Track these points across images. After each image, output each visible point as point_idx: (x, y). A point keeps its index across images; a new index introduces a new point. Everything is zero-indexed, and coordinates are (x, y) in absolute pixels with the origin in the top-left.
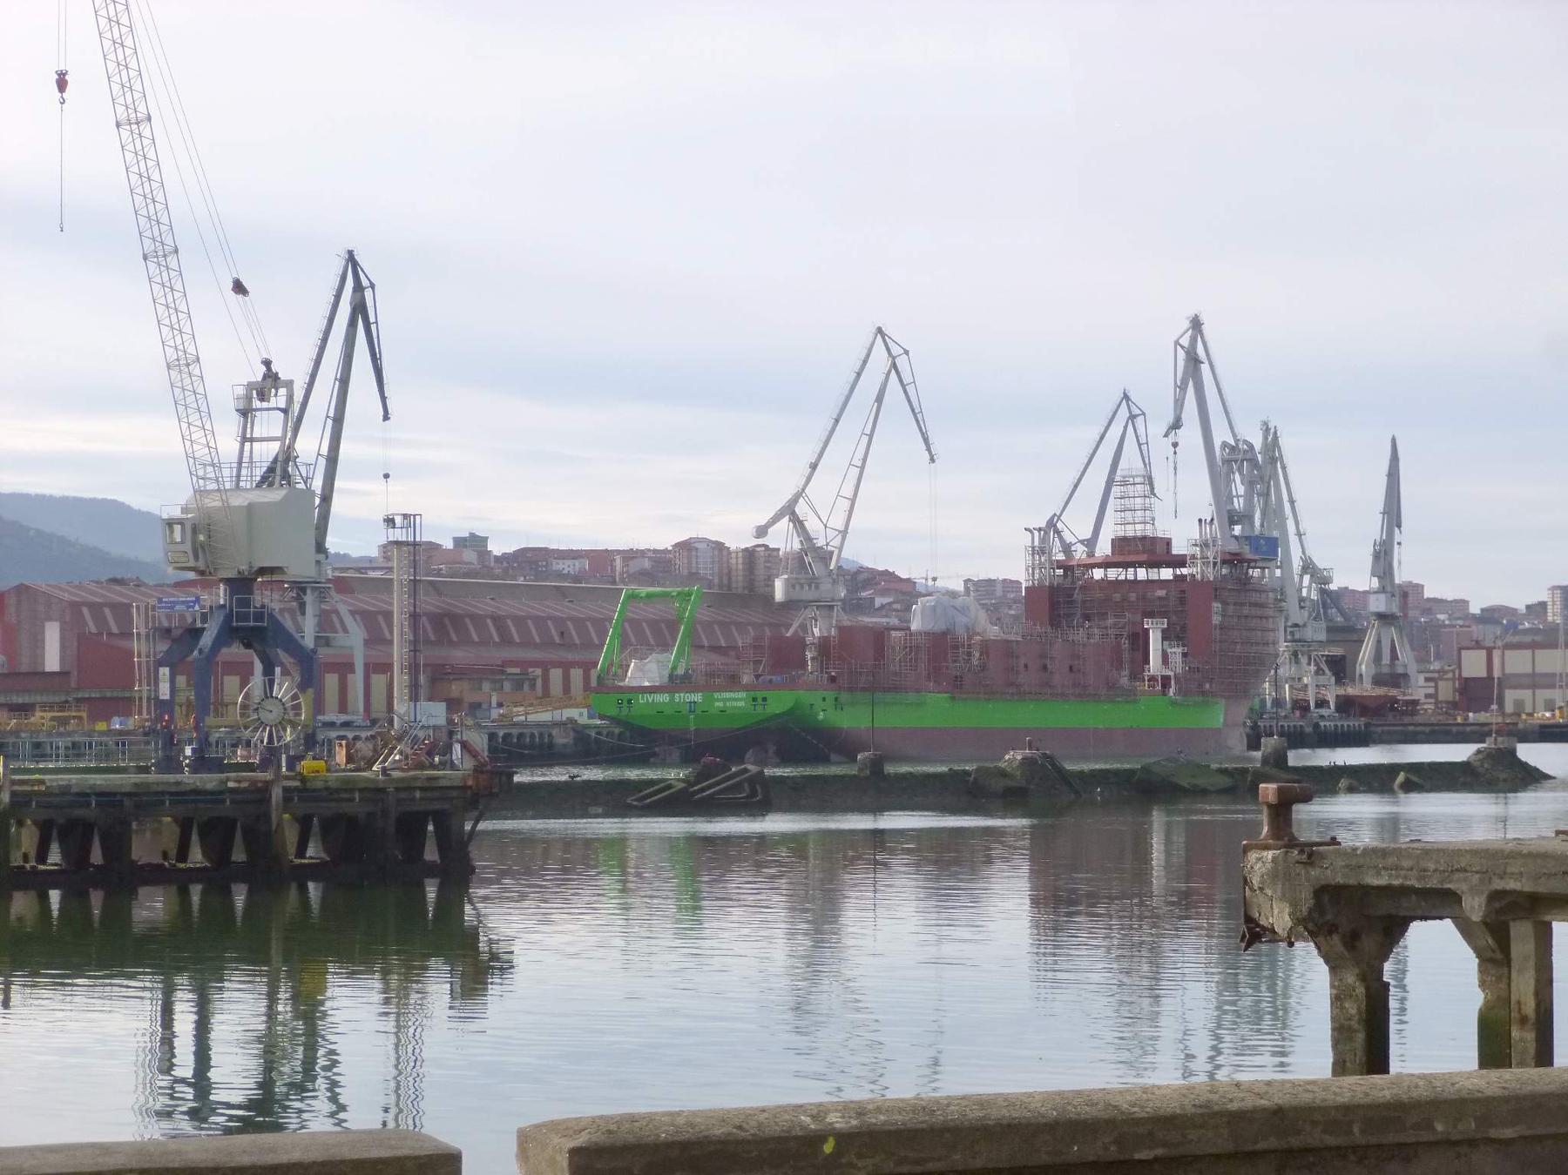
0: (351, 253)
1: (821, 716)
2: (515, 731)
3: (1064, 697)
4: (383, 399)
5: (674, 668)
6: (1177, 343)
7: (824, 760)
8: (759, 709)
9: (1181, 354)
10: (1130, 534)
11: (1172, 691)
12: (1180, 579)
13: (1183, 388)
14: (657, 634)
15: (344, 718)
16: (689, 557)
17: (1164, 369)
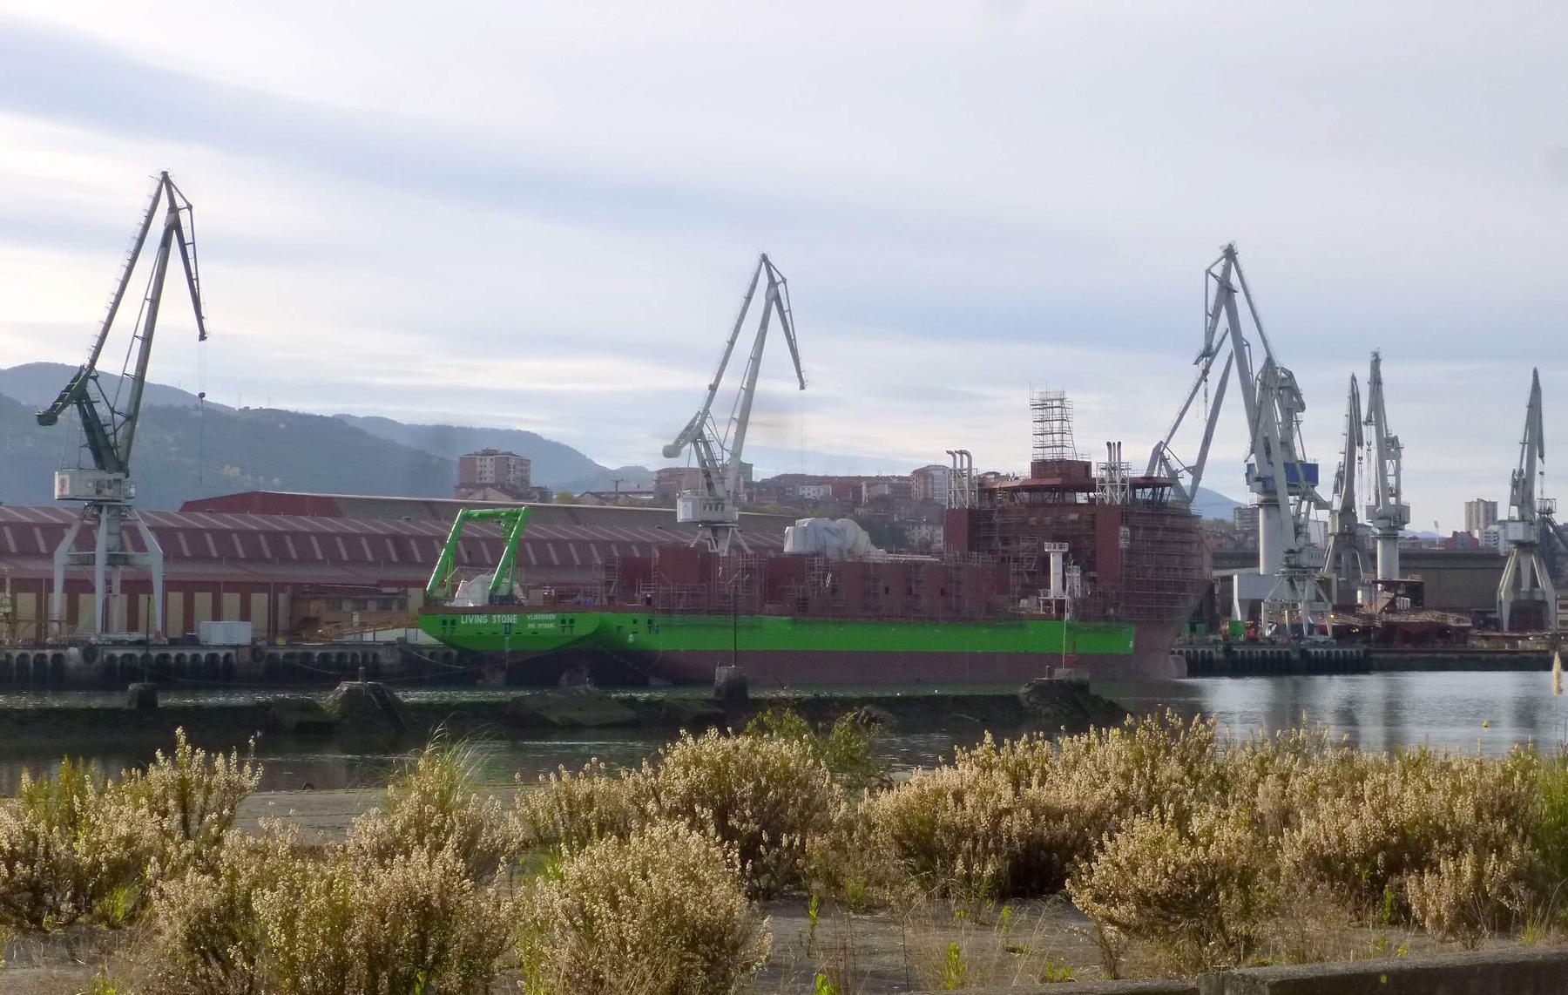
0: (165, 174)
1: (631, 638)
2: (349, 651)
3: (933, 619)
4: (200, 318)
5: (495, 588)
6: (1208, 272)
7: (643, 684)
8: (567, 631)
9: (1214, 285)
10: (1049, 457)
11: (1067, 616)
12: (1091, 501)
13: (1215, 316)
14: (474, 557)
15: (136, 636)
16: (926, 484)
17: (1197, 293)
